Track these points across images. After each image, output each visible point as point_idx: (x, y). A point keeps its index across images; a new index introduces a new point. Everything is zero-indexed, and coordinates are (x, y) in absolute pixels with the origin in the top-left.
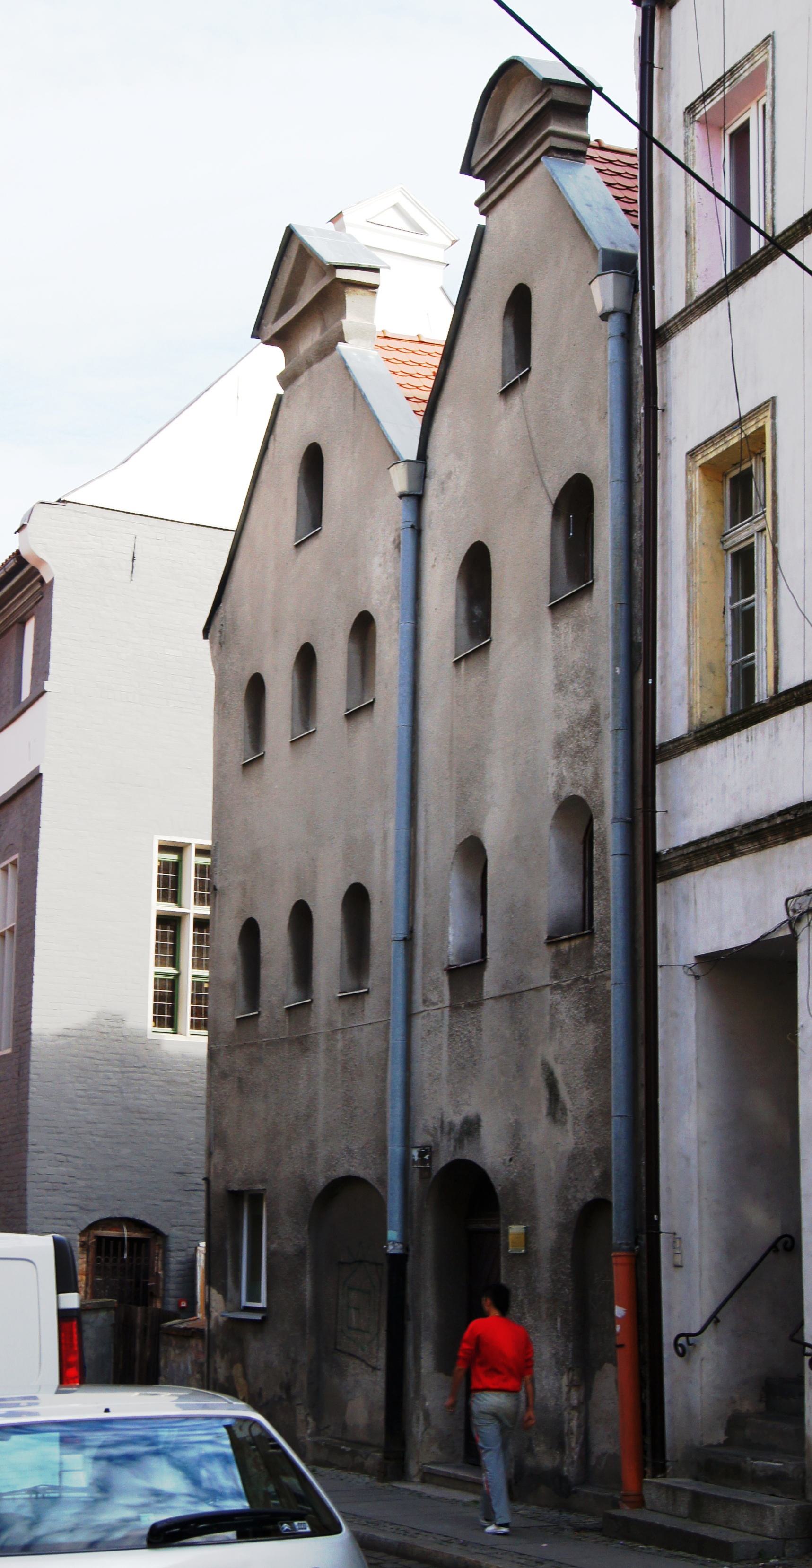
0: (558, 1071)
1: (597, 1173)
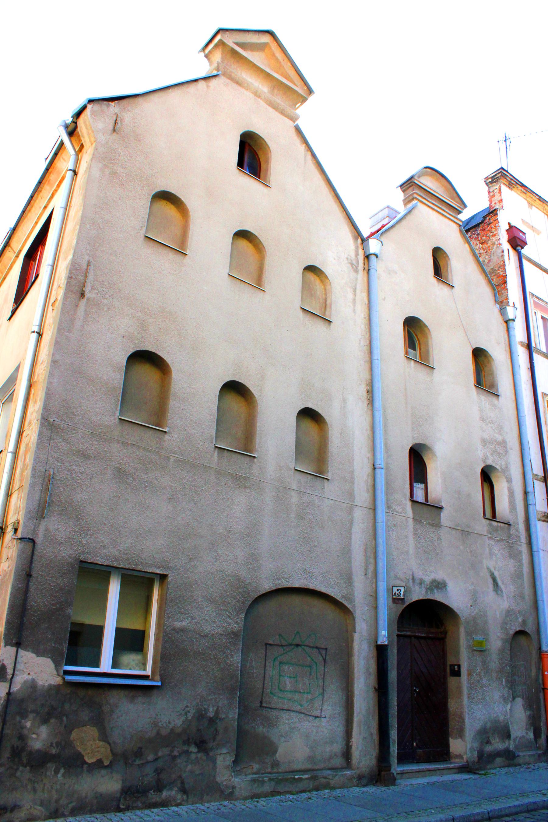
0: (496, 574)
1: (520, 620)
